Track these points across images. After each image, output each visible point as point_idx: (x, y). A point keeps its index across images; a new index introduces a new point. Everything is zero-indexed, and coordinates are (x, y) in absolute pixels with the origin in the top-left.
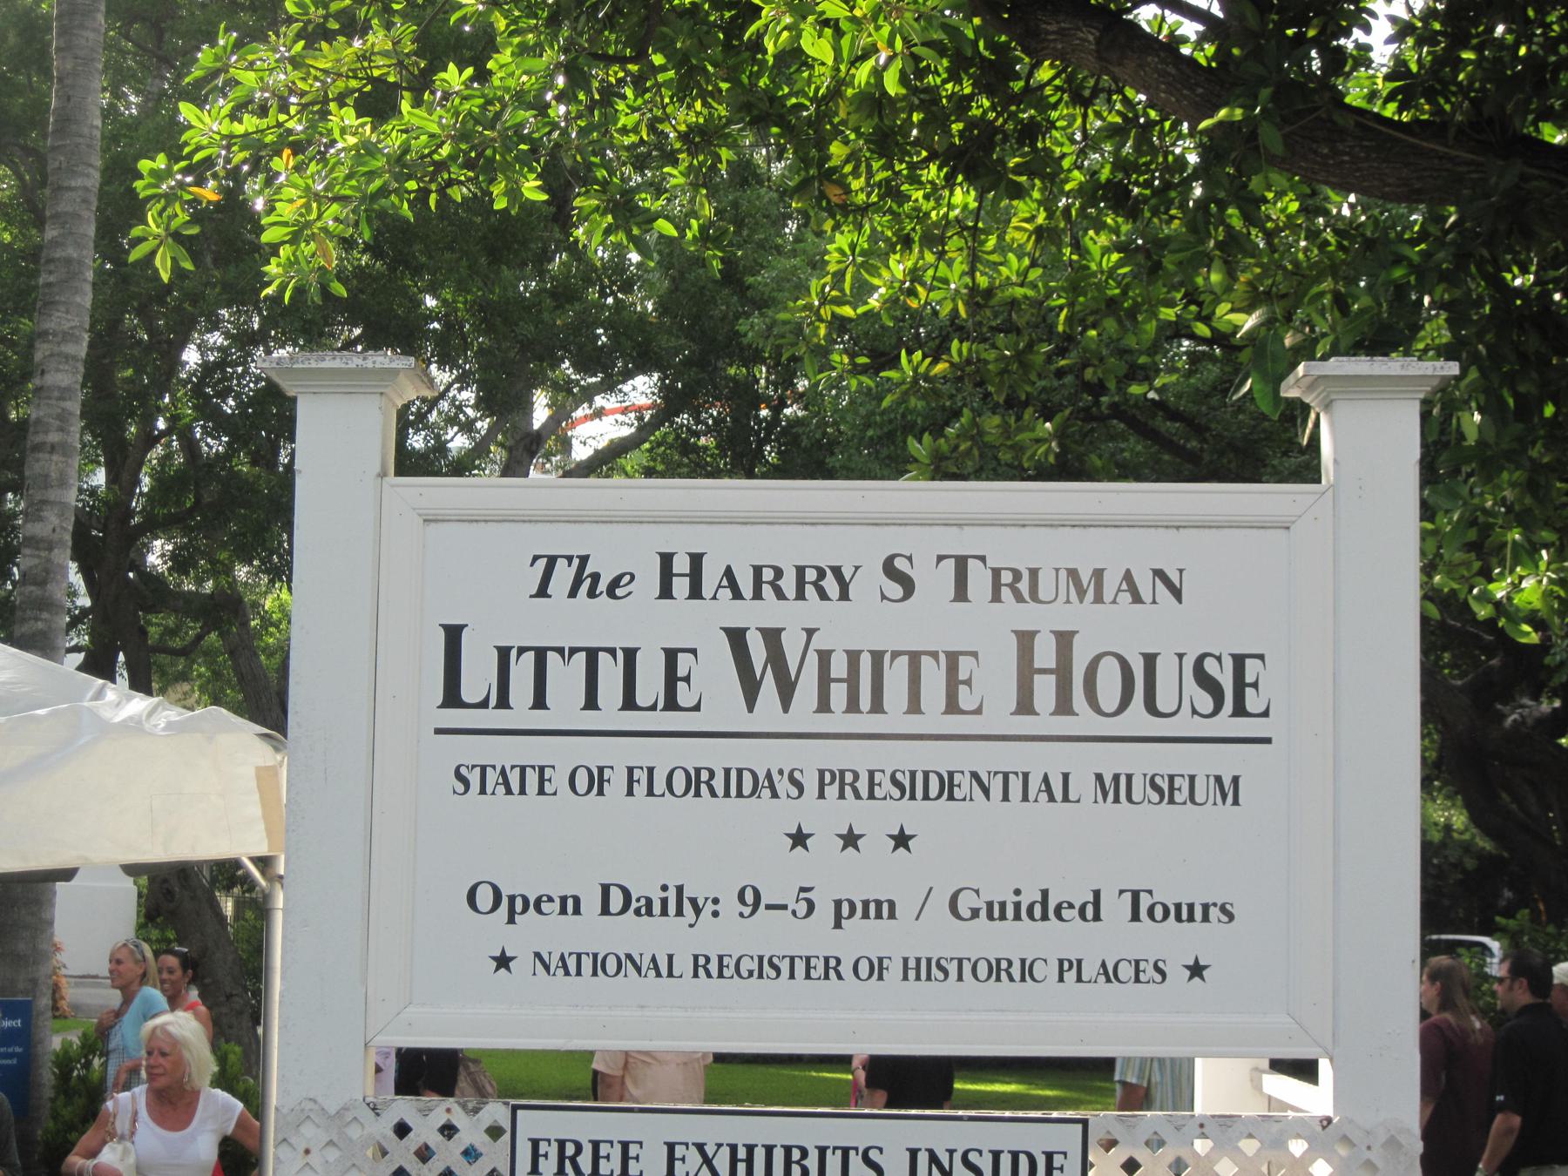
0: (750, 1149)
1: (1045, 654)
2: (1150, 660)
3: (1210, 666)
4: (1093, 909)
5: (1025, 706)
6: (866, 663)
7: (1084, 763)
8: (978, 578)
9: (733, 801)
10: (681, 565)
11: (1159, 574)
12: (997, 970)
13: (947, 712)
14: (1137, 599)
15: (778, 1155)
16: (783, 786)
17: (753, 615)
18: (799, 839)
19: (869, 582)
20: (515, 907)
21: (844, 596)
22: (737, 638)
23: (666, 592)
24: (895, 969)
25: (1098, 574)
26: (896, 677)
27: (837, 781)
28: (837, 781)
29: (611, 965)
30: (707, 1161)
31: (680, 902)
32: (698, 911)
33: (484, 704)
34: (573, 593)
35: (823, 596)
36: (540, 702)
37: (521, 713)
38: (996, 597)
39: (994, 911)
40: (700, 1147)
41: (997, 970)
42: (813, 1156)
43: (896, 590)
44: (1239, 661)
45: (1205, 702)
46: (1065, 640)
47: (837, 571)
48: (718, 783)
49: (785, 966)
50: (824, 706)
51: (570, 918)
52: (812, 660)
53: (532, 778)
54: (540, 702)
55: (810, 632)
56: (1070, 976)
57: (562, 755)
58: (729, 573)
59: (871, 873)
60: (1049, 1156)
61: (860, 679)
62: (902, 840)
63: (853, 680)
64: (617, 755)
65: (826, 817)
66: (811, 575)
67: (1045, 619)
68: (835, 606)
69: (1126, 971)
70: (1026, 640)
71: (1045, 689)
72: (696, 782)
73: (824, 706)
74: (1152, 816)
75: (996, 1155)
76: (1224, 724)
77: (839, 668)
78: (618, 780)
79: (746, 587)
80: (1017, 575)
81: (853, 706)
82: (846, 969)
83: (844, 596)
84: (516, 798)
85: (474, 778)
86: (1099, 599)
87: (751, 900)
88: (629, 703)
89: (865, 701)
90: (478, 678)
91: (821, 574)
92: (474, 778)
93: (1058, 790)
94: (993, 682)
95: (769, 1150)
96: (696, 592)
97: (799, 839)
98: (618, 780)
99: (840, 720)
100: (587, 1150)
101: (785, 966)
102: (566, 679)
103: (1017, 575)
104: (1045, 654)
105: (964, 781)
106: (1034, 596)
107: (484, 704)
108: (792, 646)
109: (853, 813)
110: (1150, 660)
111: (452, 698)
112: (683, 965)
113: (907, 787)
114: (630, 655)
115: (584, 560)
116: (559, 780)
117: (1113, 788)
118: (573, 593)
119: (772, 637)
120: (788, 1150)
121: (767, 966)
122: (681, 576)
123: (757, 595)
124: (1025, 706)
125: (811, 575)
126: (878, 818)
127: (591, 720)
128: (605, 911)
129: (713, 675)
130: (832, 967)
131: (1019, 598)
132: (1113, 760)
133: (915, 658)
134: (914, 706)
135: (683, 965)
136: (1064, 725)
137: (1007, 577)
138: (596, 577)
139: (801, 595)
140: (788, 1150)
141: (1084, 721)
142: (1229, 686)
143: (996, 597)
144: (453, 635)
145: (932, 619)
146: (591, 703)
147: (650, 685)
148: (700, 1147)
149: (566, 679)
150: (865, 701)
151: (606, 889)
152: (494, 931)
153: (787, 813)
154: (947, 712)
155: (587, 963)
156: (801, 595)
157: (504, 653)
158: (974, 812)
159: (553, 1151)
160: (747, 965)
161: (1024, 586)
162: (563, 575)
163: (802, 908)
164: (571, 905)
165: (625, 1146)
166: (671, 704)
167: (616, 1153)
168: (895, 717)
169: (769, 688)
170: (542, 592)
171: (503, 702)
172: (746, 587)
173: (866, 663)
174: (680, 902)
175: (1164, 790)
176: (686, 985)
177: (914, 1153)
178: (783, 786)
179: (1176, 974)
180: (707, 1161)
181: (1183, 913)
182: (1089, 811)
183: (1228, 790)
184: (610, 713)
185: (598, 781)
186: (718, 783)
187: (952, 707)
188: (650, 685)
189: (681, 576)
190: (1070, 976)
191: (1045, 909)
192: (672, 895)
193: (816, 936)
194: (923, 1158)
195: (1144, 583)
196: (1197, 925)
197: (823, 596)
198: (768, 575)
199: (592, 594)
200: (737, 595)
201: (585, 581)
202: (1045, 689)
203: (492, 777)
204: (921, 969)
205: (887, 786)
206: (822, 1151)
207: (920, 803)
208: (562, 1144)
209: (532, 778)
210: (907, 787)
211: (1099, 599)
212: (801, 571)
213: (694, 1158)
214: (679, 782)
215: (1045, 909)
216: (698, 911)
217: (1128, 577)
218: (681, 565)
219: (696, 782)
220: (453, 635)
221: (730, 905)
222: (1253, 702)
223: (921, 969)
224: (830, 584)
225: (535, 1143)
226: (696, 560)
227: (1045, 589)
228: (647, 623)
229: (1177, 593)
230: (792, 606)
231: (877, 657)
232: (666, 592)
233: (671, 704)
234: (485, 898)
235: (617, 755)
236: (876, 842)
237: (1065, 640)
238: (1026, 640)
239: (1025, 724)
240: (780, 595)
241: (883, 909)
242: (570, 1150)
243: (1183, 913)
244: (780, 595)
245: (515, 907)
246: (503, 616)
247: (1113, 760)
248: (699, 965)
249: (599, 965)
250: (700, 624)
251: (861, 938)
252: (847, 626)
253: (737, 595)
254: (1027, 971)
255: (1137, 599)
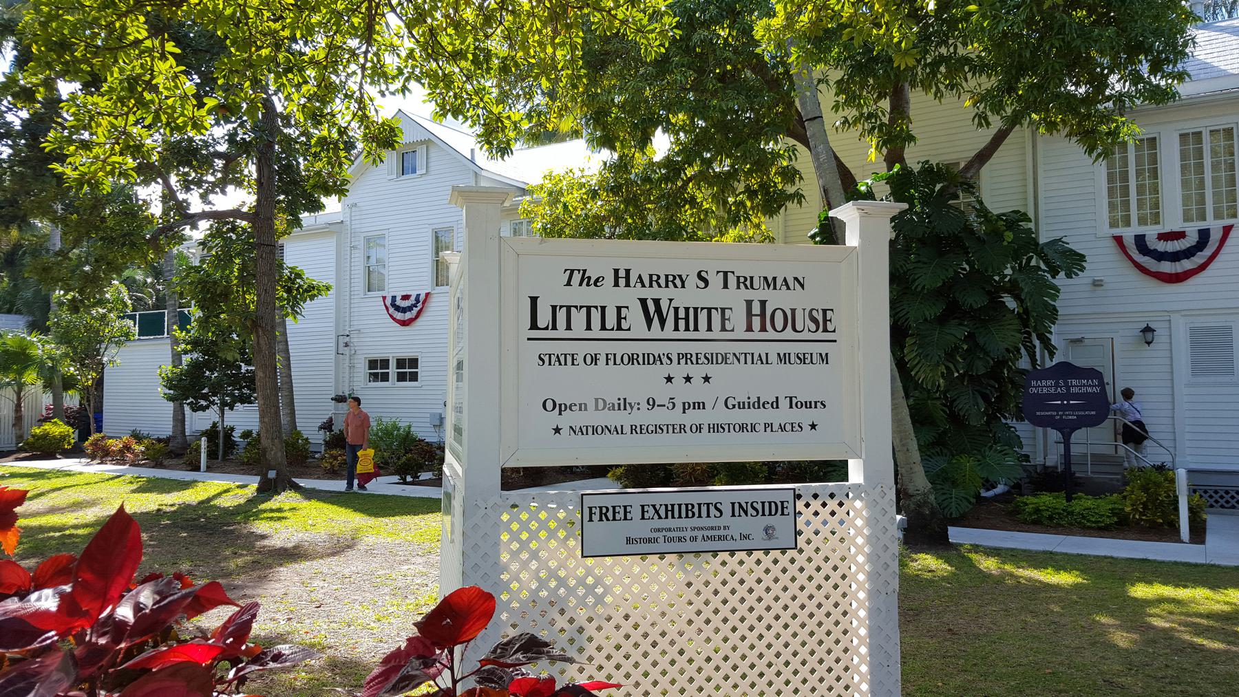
0: (673, 506)
1: (756, 309)
2: (793, 311)
3: (814, 313)
4: (776, 404)
5: (749, 329)
6: (691, 312)
7: (774, 349)
8: (732, 280)
9: (646, 366)
10: (622, 273)
11: (796, 279)
12: (742, 428)
13: (531, 329)
14: (788, 288)
15: (683, 507)
16: (665, 360)
17: (650, 293)
18: (669, 379)
19: (692, 281)
20: (561, 408)
21: (683, 286)
22: (643, 302)
23: (616, 284)
24: (705, 428)
25: (774, 279)
26: (703, 317)
27: (685, 357)
28: (685, 357)
29: (600, 430)
30: (657, 512)
31: (624, 405)
32: (632, 408)
33: (547, 328)
34: (581, 285)
35: (676, 286)
36: (569, 328)
37: (561, 332)
38: (738, 287)
39: (741, 406)
40: (654, 506)
41: (742, 428)
42: (696, 507)
43: (702, 284)
44: (825, 311)
45: (813, 327)
46: (763, 303)
47: (680, 276)
48: (640, 360)
49: (665, 428)
50: (676, 329)
51: (583, 412)
52: (672, 311)
53: (569, 358)
54: (569, 328)
55: (671, 300)
56: (769, 429)
57: (581, 349)
58: (640, 277)
59: (696, 391)
60: (782, 503)
61: (689, 318)
62: (707, 379)
63: (687, 319)
64: (602, 349)
65: (678, 371)
66: (671, 278)
67: (756, 296)
68: (680, 290)
69: (788, 427)
70: (749, 303)
71: (756, 322)
72: (632, 359)
73: (676, 329)
74: (797, 369)
75: (763, 503)
76: (820, 335)
77: (682, 314)
78: (602, 359)
79: (647, 283)
80: (746, 279)
81: (687, 329)
82: (688, 429)
83: (683, 286)
84: (563, 367)
85: (546, 359)
86: (775, 288)
87: (652, 403)
88: (603, 328)
89: (692, 326)
90: (544, 318)
91: (674, 277)
92: (546, 359)
93: (764, 360)
94: (738, 319)
95: (680, 505)
96: (628, 285)
97: (669, 379)
98: (602, 359)
99: (682, 334)
100: (611, 510)
101: (665, 428)
102: (579, 318)
103: (746, 279)
104: (756, 309)
105: (730, 356)
106: (752, 287)
107: (547, 328)
108: (664, 305)
109: (690, 369)
110: (793, 311)
111: (534, 326)
112: (627, 429)
113: (710, 359)
114: (603, 308)
115: (585, 271)
116: (580, 359)
117: (784, 358)
118: (581, 285)
119: (657, 302)
120: (687, 505)
121: (658, 429)
122: (622, 278)
123: (651, 286)
124: (749, 329)
125: (671, 278)
126: (697, 371)
127: (589, 334)
128: (597, 409)
129: (635, 317)
130: (682, 428)
131: (746, 287)
132: (784, 348)
133: (709, 310)
134: (710, 329)
135: (627, 429)
136: (763, 336)
137: (742, 280)
138: (589, 278)
139: (667, 286)
140: (687, 505)
141: (770, 334)
142: (822, 320)
143: (738, 287)
144: (534, 300)
145: (714, 296)
146: (589, 328)
147: (611, 321)
148: (654, 506)
149: (579, 318)
150: (692, 326)
151: (597, 400)
152: (553, 418)
153: (666, 370)
154: (531, 329)
155: (590, 430)
156: (667, 286)
157: (554, 308)
158: (736, 368)
159: (598, 511)
160: (650, 428)
161: (748, 283)
162: (577, 277)
163: (671, 406)
164: (583, 407)
165: (625, 507)
166: (619, 328)
167: (622, 511)
168: (703, 333)
169: (656, 321)
170: (569, 284)
171: (554, 328)
172: (647, 283)
173: (691, 312)
174: (624, 405)
175: (802, 359)
176: (629, 438)
177: (733, 504)
178: (665, 360)
179: (807, 428)
180: (657, 512)
181: (808, 405)
182: (776, 368)
183: (824, 358)
184: (596, 332)
185: (595, 359)
186: (640, 360)
187: (723, 329)
188: (611, 321)
189: (622, 278)
190: (769, 429)
191: (759, 404)
192: (622, 402)
193: (676, 417)
194: (737, 506)
195: (791, 282)
196: (813, 409)
197: (676, 286)
198: (655, 278)
199: (588, 285)
200: (643, 286)
201: (585, 280)
202: (756, 322)
203: (553, 358)
204: (716, 428)
205: (703, 359)
206: (699, 505)
207: (714, 365)
208: (601, 508)
209: (569, 358)
210: (710, 359)
211: (775, 288)
212: (667, 276)
213: (652, 511)
214: (626, 359)
215: (759, 404)
216: (632, 408)
217: (785, 280)
218: (622, 273)
219: (632, 359)
220: (534, 300)
221: (644, 405)
222: (830, 327)
223: (716, 428)
224: (678, 282)
225: (590, 508)
226: (628, 271)
227: (756, 285)
228: (609, 296)
229: (802, 286)
230: (647, 289)
231: (696, 309)
232: (616, 284)
233: (619, 328)
234: (549, 405)
235: (602, 349)
236: (697, 380)
237: (763, 303)
238: (749, 303)
239: (749, 335)
240: (660, 286)
241: (700, 405)
242: (604, 510)
243: (808, 405)
244: (660, 286)
245: (561, 408)
246: (554, 293)
247: (784, 348)
248: (633, 429)
249: (595, 431)
250: (630, 297)
251: (693, 417)
252: (688, 297)
253: (643, 286)
254: (753, 428)
255: (788, 288)
